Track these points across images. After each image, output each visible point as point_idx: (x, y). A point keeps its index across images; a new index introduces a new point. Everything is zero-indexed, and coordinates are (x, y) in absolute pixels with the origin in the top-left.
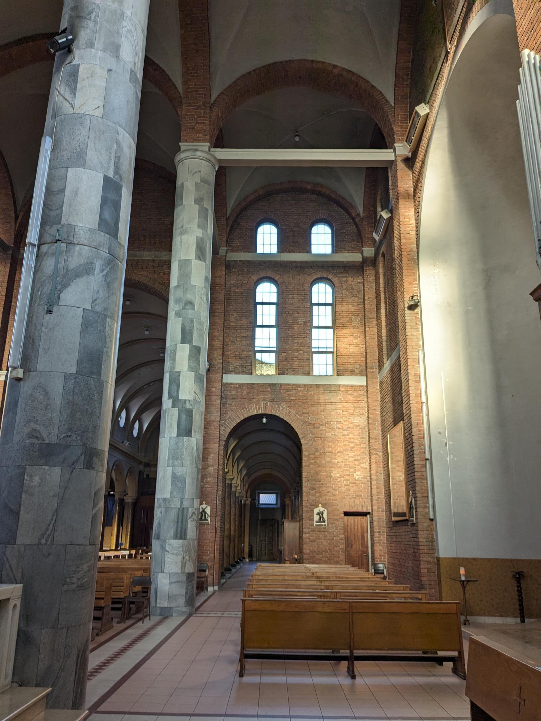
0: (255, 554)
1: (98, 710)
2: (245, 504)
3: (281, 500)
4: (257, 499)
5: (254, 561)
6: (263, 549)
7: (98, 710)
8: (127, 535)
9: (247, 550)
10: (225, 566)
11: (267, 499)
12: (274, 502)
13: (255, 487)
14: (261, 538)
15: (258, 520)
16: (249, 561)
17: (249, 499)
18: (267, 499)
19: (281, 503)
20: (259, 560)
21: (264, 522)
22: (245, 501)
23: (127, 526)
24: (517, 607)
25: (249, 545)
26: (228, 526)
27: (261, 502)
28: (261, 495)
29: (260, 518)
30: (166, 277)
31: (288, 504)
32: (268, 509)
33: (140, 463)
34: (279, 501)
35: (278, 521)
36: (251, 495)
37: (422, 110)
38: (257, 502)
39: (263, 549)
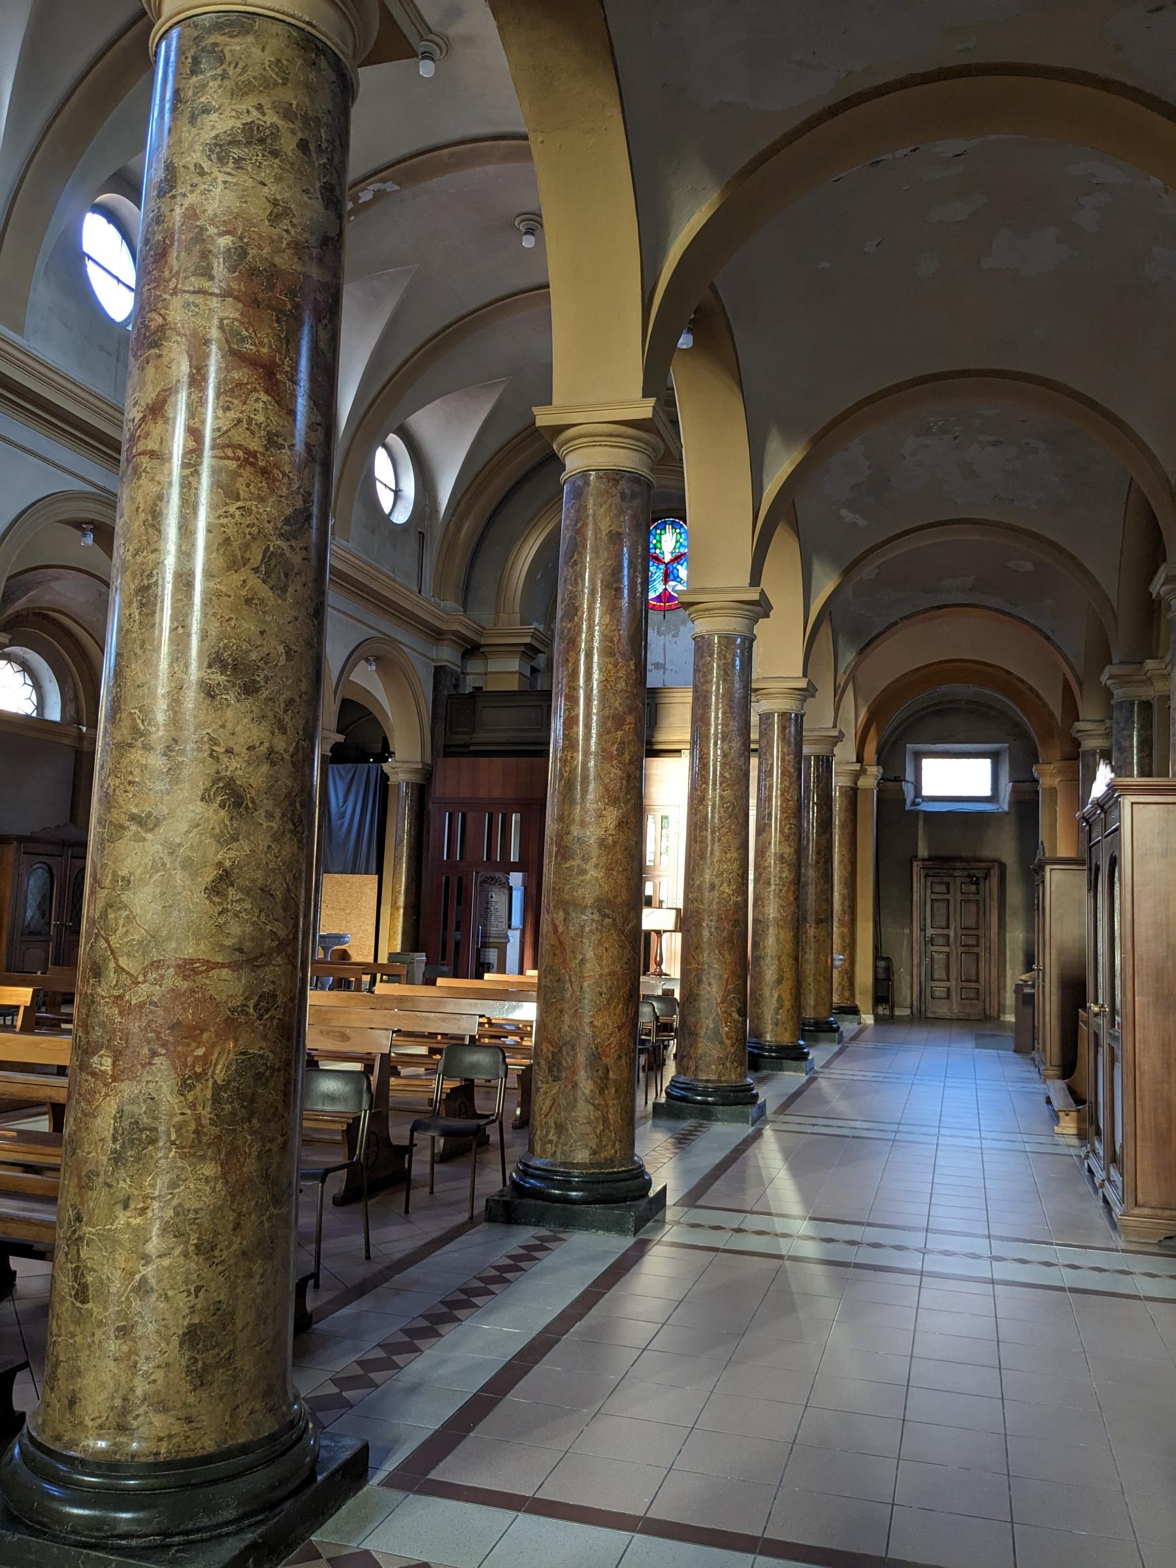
0: (905, 991)
1: (432, 1476)
2: (855, 790)
3: (1015, 781)
4: (909, 776)
5: (901, 1021)
6: (939, 973)
7: (432, 1476)
8: (394, 906)
9: (865, 976)
10: (835, 999)
11: (956, 778)
12: (987, 792)
13: (911, 720)
14: (930, 932)
15: (915, 857)
16: (878, 1019)
17: (874, 771)
18: (956, 778)
19: (1014, 791)
20: (921, 1018)
21: (940, 864)
22: (857, 776)
23: (395, 874)
24: (216, 1477)
25: (877, 956)
26: (612, 816)
27: (926, 792)
28: (927, 764)
29: (923, 852)
30: (77, 862)
31: (1053, 791)
32: (961, 819)
33: (436, 635)
34: (1006, 787)
35: (1002, 867)
36: (879, 752)
37: (340, 738)
38: (908, 789)
39: (939, 973)
